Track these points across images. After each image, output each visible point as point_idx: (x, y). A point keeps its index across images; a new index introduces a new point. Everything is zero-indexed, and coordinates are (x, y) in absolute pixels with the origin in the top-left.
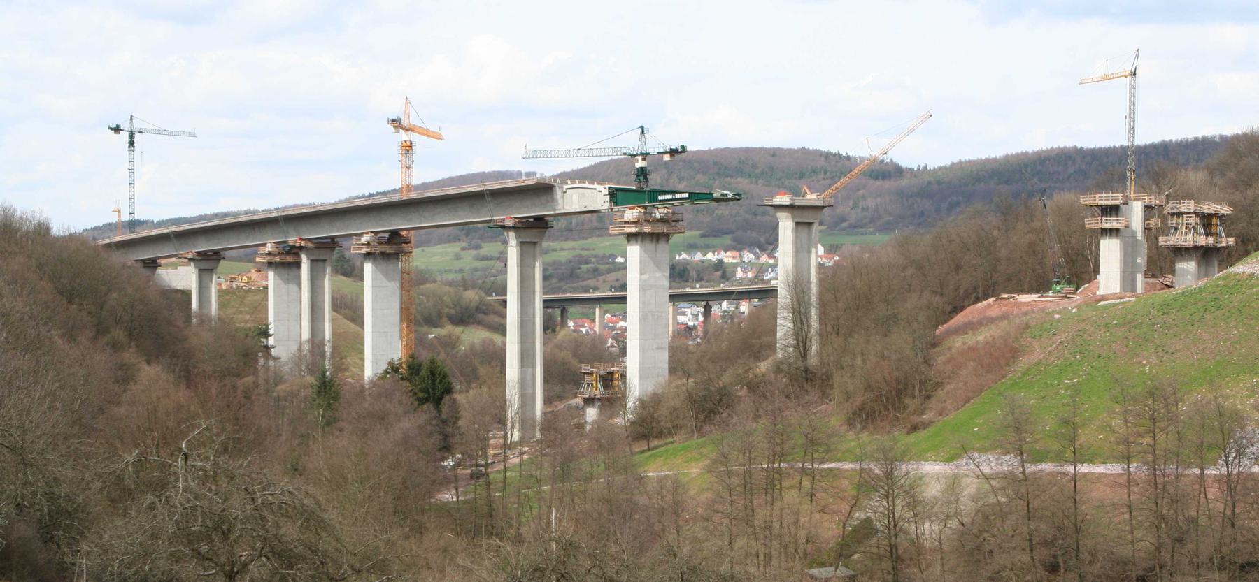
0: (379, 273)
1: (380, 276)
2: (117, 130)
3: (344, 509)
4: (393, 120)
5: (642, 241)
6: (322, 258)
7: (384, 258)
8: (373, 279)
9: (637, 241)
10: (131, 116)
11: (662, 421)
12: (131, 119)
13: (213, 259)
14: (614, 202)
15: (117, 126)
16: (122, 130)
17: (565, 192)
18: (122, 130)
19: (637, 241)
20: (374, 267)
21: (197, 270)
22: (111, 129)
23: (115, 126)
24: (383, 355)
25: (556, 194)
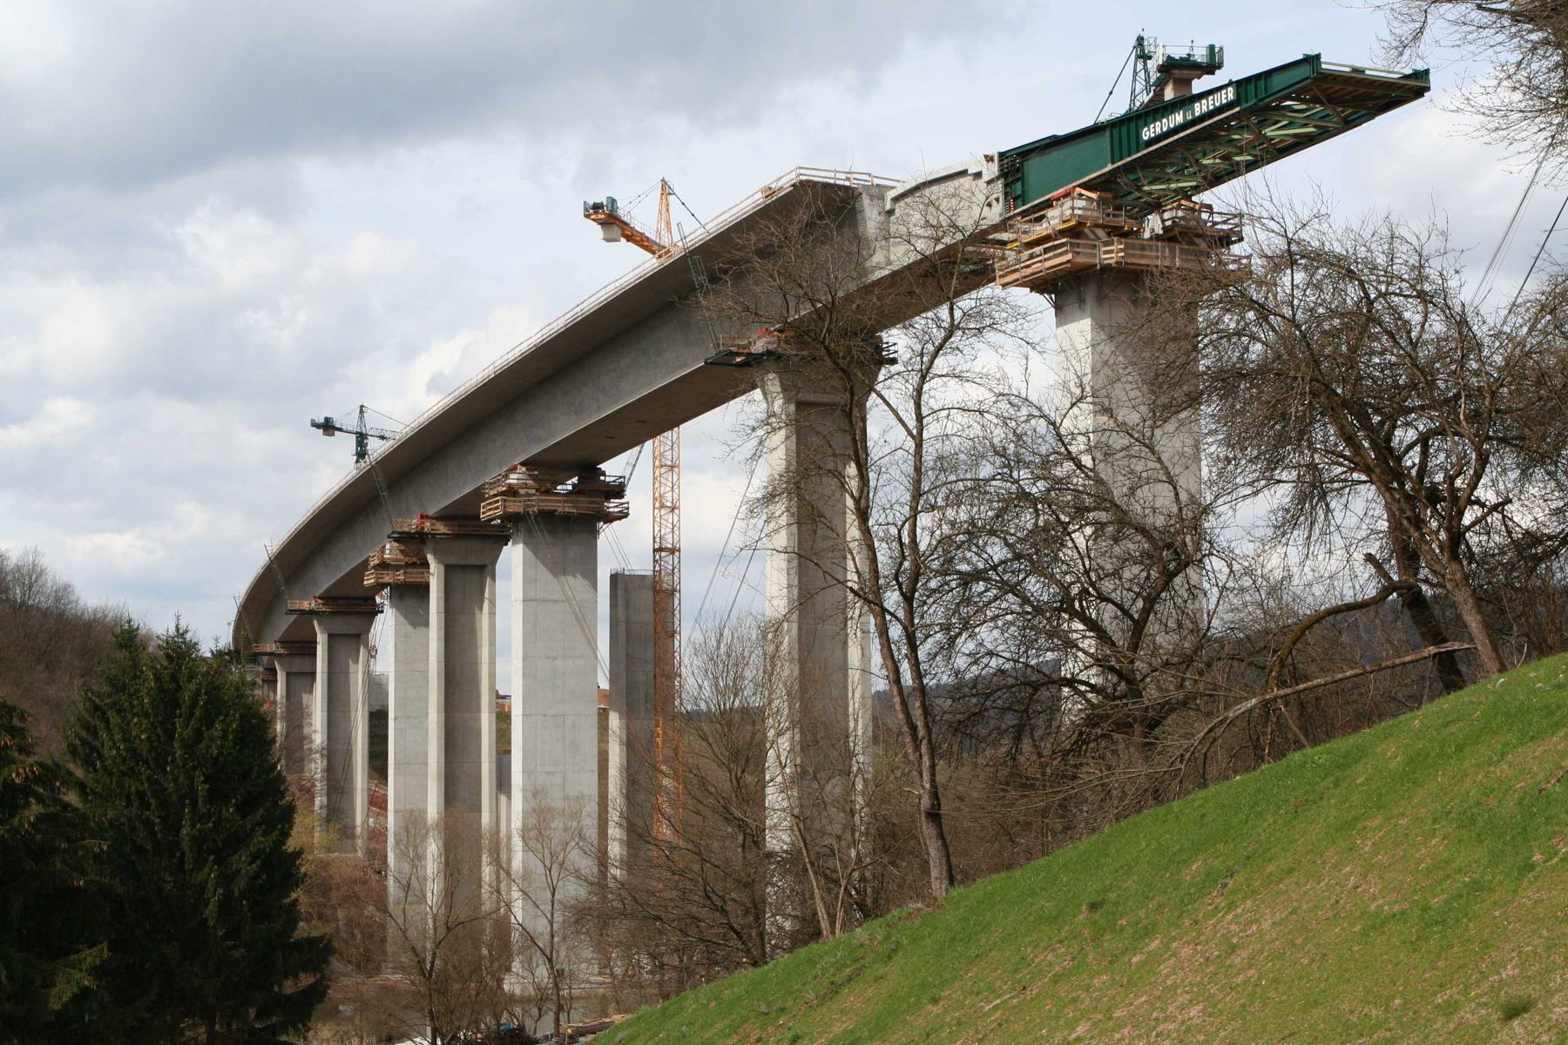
0: (541, 567)
1: (544, 573)
2: (328, 427)
3: (1541, 983)
4: (597, 207)
5: (1101, 299)
6: (473, 561)
7: (553, 532)
8: (527, 580)
9: (1082, 301)
10: (362, 407)
11: (782, 847)
12: (361, 412)
13: (358, 613)
14: (1015, 199)
15: (327, 419)
16: (340, 430)
17: (891, 212)
18: (340, 430)
19: (1082, 301)
20: (529, 553)
21: (326, 635)
22: (315, 425)
23: (322, 421)
24: (553, 773)
25: (864, 219)
